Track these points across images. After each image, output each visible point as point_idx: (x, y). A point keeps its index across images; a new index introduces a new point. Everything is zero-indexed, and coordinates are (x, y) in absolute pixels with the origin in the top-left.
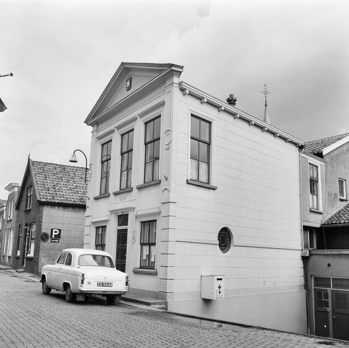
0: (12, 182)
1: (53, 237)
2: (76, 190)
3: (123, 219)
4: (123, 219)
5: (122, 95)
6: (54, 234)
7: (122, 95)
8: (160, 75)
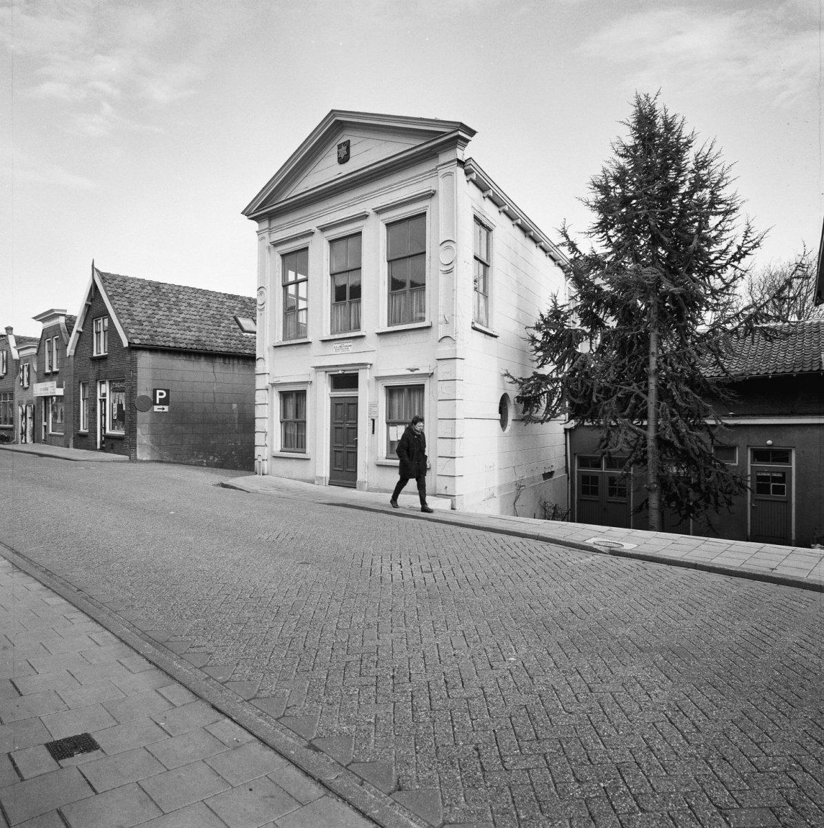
0: (53, 308)
1: (158, 402)
2: (186, 324)
3: (345, 380)
4: (345, 380)
5: (327, 170)
6: (158, 397)
7: (327, 170)
8: (433, 140)
